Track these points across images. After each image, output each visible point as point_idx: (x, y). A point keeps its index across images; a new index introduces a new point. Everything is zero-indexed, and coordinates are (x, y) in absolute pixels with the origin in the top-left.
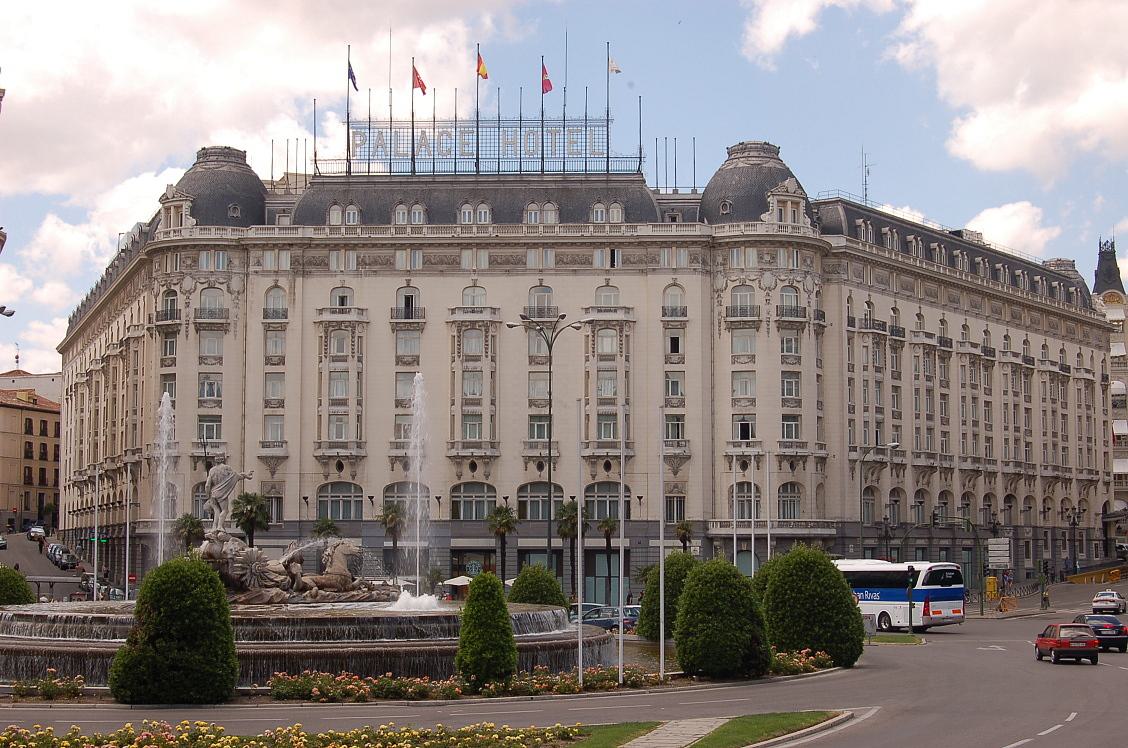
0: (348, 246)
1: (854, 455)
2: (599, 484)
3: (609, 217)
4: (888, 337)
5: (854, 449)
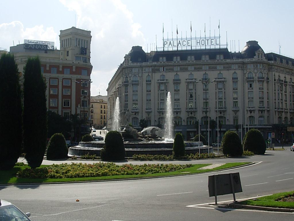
1: (276, 110)
5: (276, 108)
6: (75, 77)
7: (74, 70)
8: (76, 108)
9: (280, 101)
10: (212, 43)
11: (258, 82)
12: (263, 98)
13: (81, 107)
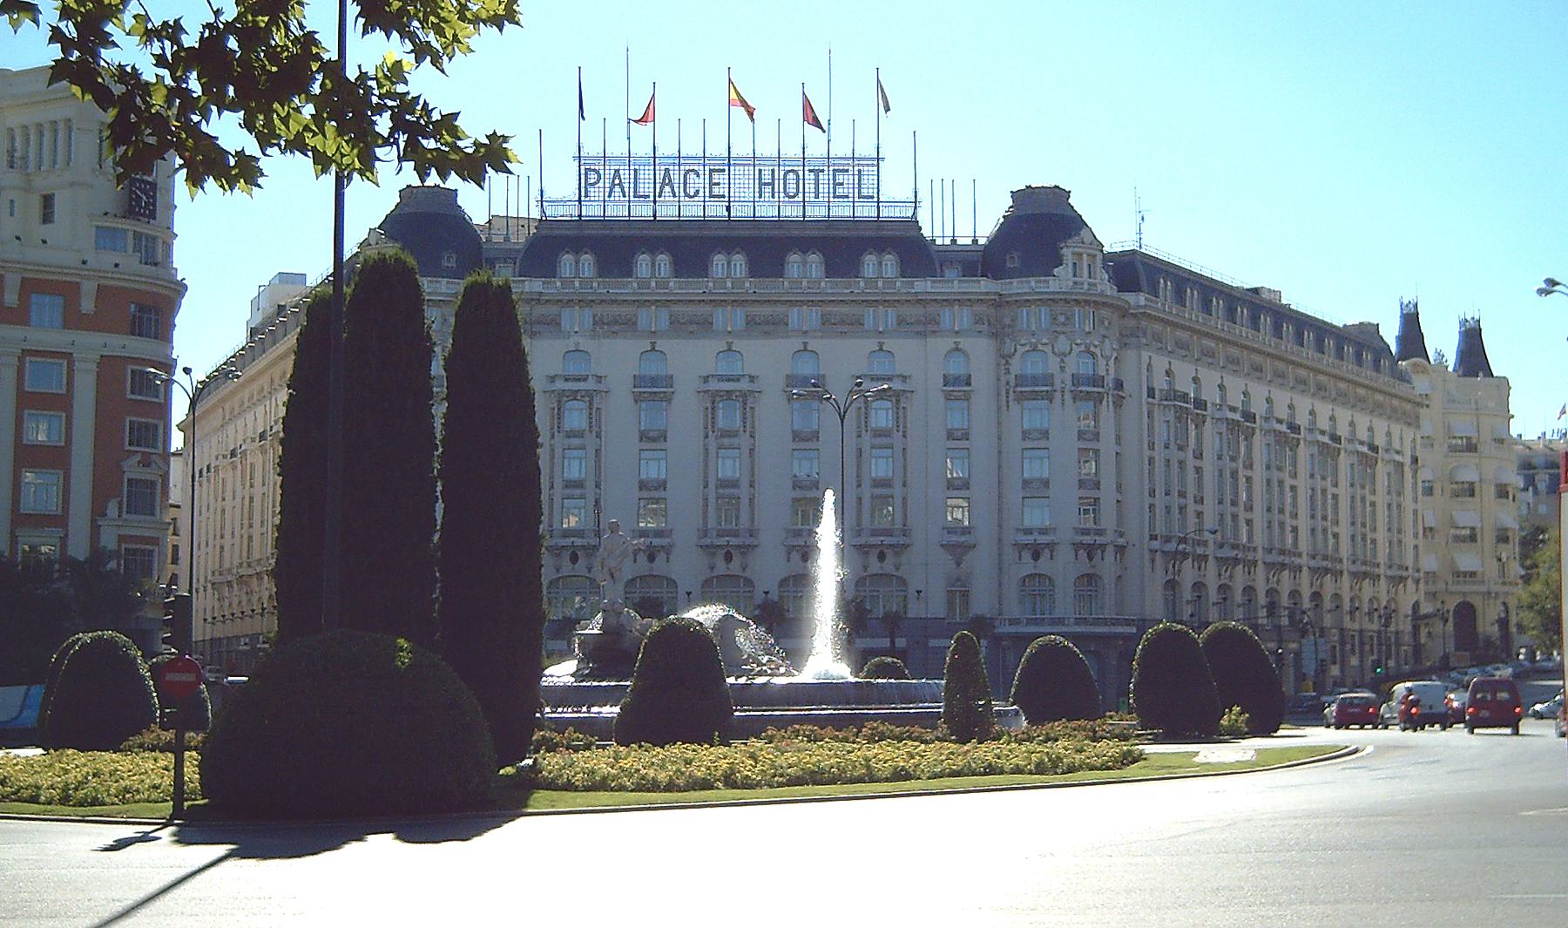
0: (583, 303)
1: (1156, 544)
2: (717, 577)
3: (879, 268)
4: (1189, 409)
5: (1153, 538)
6: (91, 345)
7: (88, 305)
8: (93, 521)
9: (1176, 501)
10: (840, 191)
11: (1074, 399)
12: (1097, 485)
13: (124, 515)
